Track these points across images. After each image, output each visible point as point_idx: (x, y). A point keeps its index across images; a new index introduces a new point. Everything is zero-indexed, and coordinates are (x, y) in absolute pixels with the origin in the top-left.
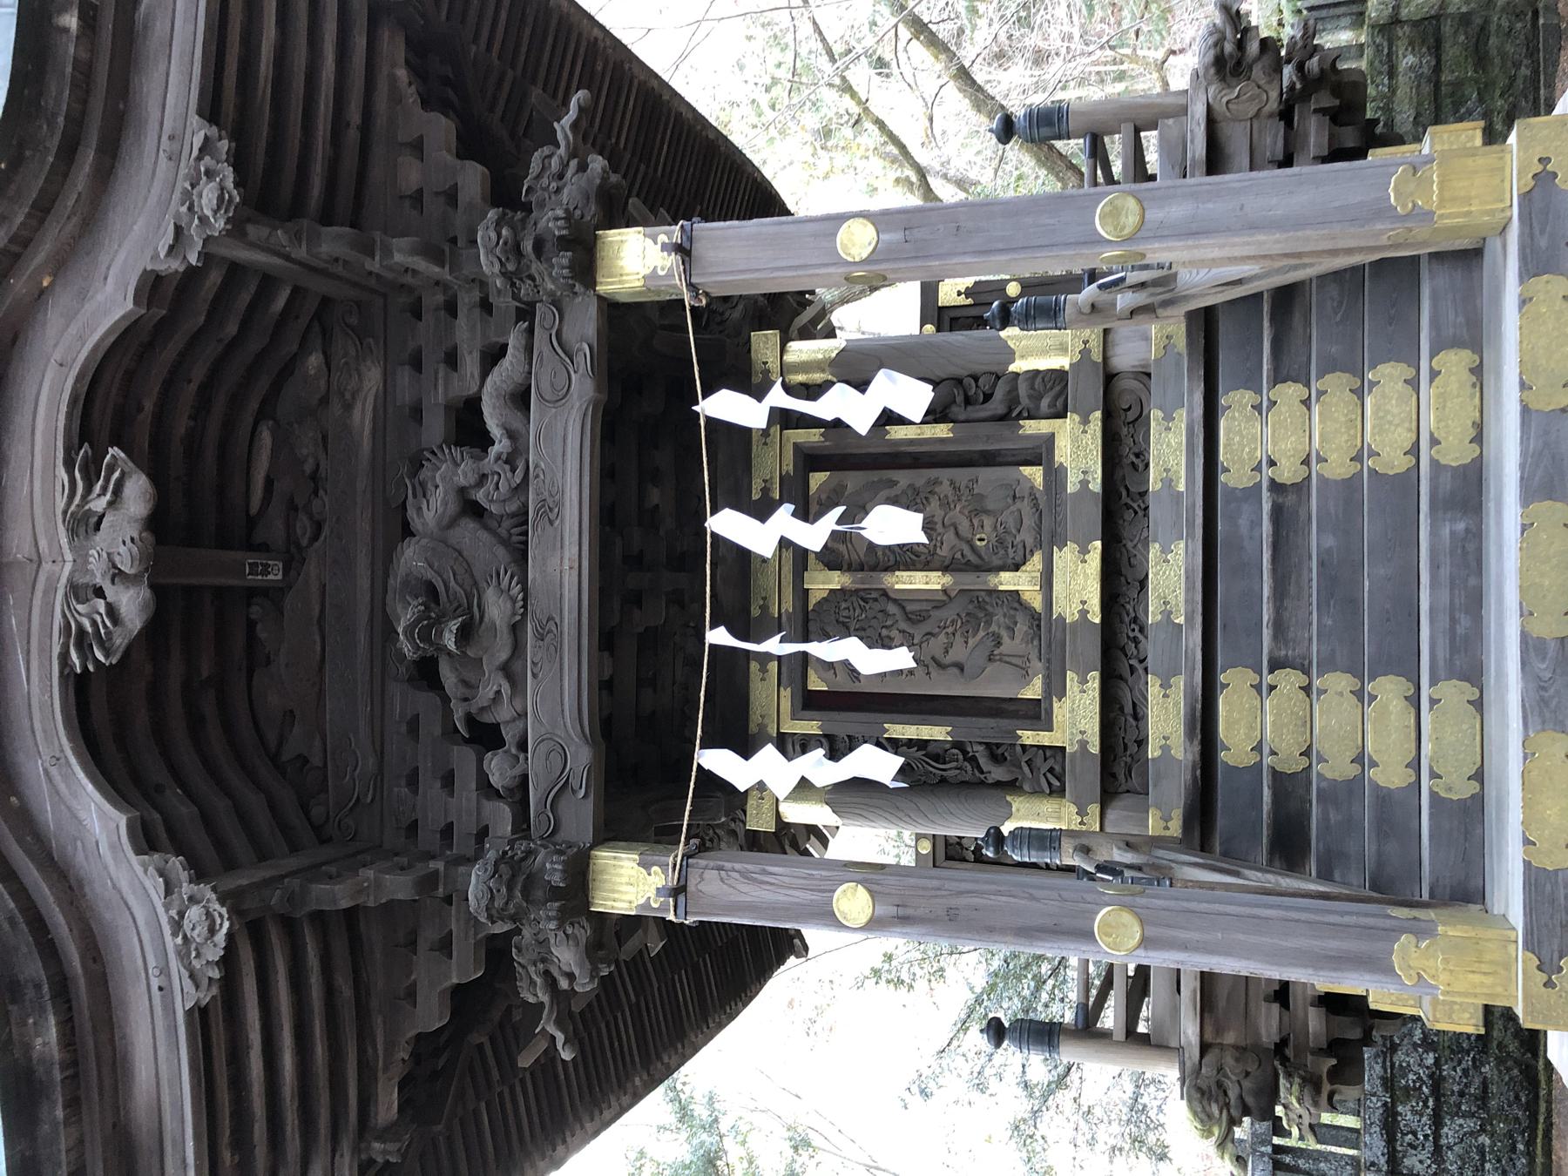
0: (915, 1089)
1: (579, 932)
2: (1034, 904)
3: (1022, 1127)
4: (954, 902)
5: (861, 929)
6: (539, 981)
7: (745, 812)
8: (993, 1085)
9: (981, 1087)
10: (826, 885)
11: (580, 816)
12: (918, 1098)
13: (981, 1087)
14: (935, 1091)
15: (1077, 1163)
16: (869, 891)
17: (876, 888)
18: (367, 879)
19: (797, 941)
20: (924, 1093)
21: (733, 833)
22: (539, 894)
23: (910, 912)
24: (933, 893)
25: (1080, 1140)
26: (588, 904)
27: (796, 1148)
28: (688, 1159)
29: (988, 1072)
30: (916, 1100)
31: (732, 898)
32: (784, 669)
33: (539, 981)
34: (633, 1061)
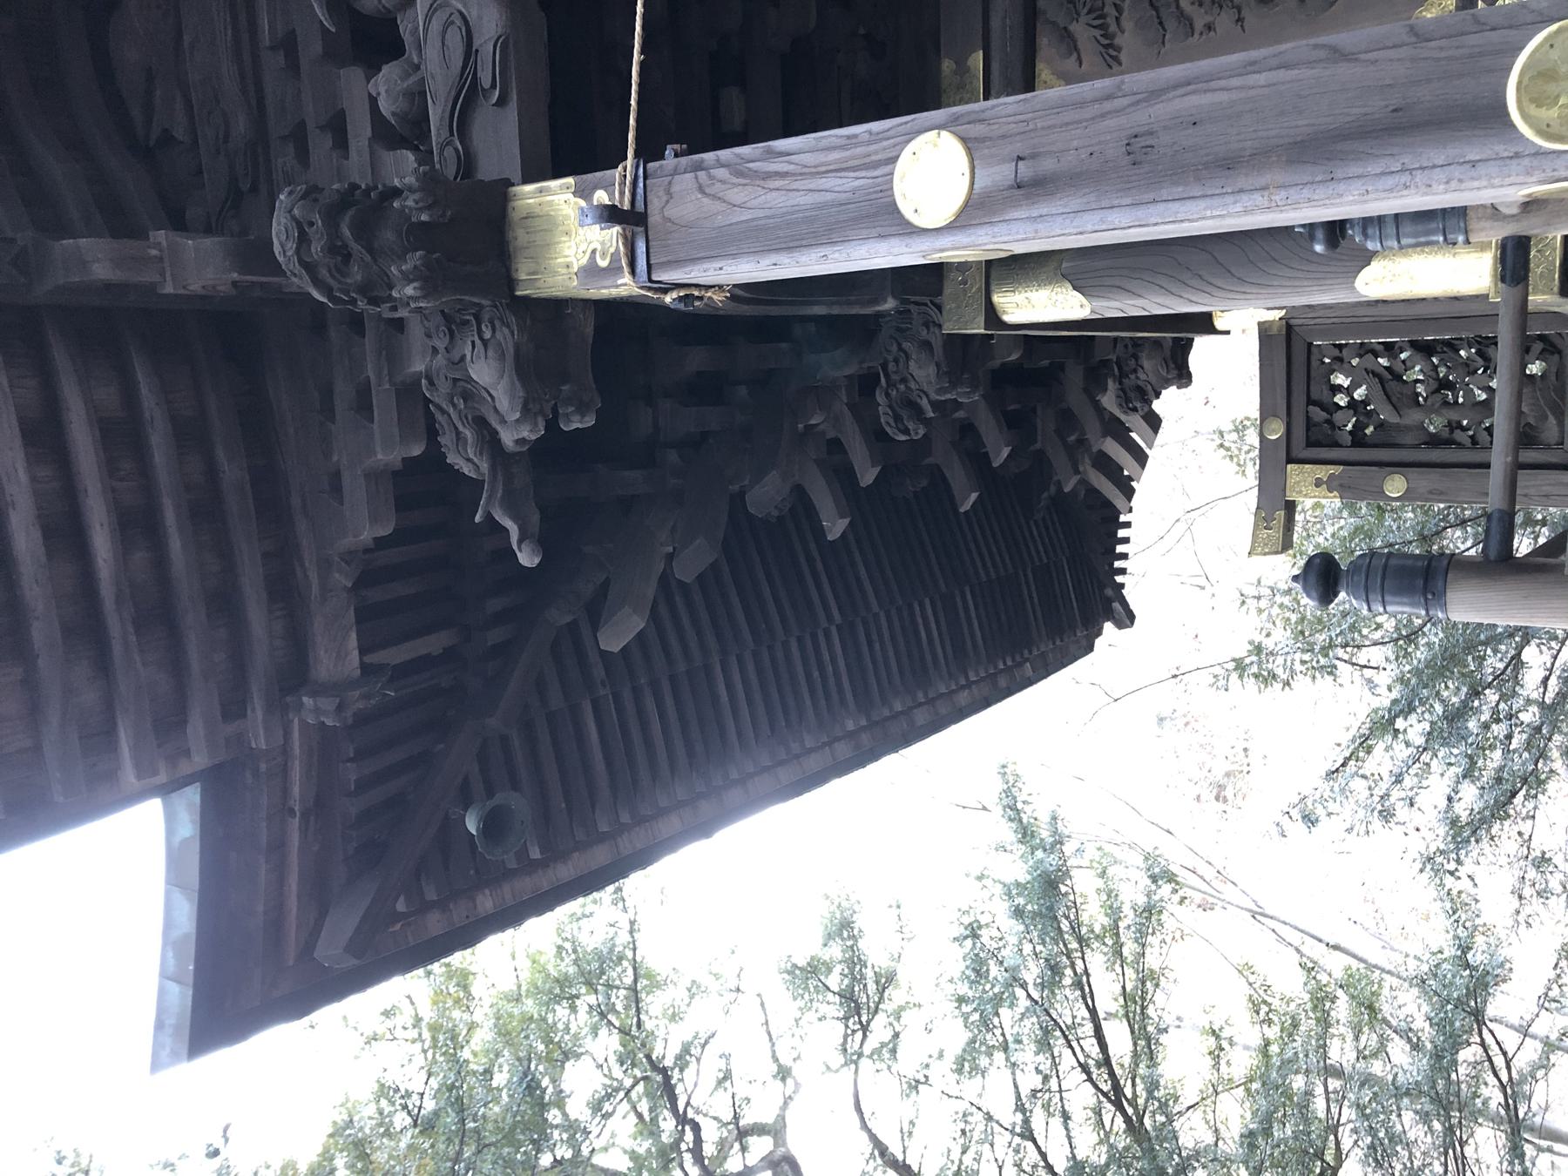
0: (1295, 813)
1: (503, 334)
2: (1344, 71)
3: (1439, 860)
4: (1141, 118)
5: (950, 228)
6: (468, 433)
7: (939, 308)
8: (1402, 812)
9: (1387, 815)
10: (878, 151)
11: (499, 136)
12: (1301, 826)
13: (1387, 815)
14: (1323, 818)
15: (1521, 918)
16: (964, 140)
17: (978, 130)
18: (158, 245)
19: (1116, 605)
20: (1310, 820)
21: (927, 345)
22: (388, 236)
23: (1048, 165)
24: (1096, 109)
25: (1527, 891)
26: (511, 283)
27: (1154, 879)
28: (1023, 878)
29: (1396, 794)
30: (1297, 828)
31: (720, 220)
32: (995, 67)
33: (468, 433)
34: (840, 691)
